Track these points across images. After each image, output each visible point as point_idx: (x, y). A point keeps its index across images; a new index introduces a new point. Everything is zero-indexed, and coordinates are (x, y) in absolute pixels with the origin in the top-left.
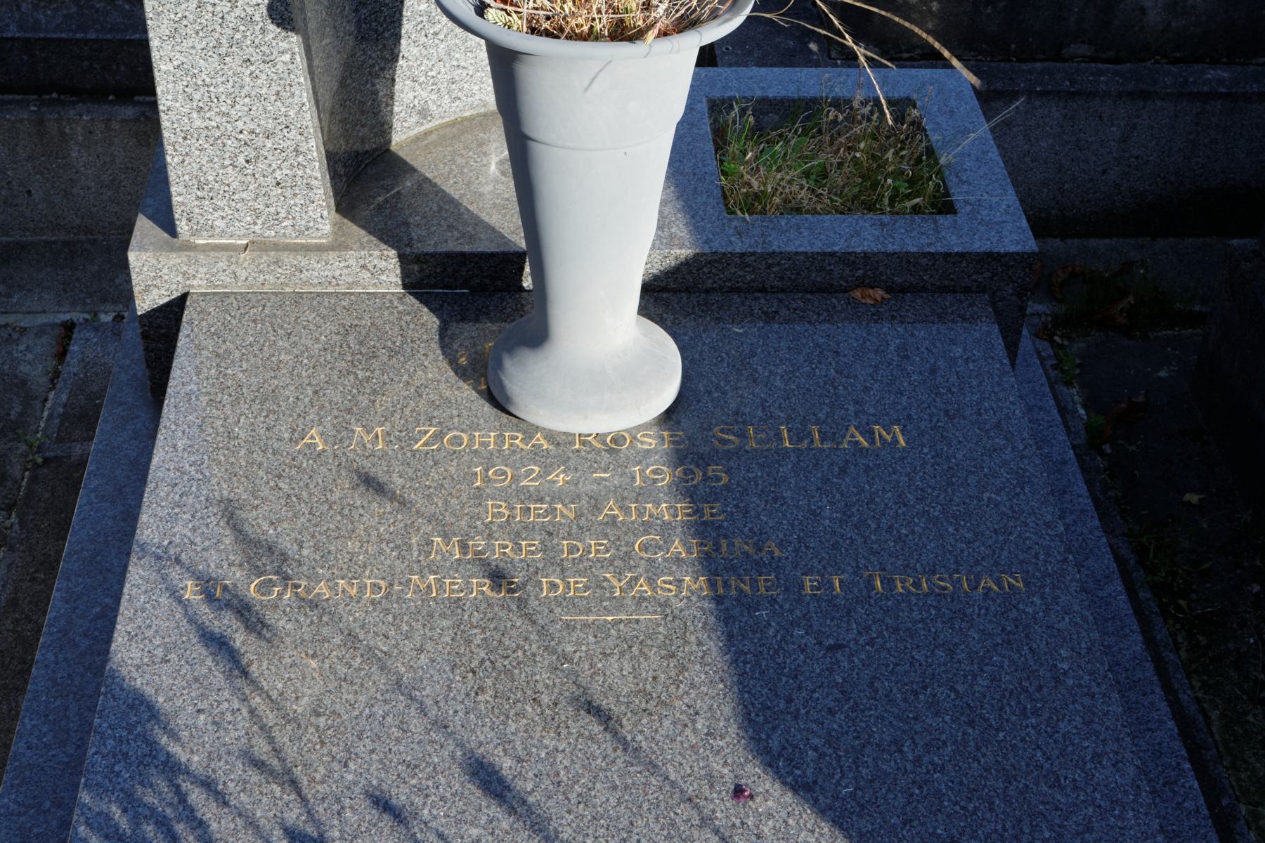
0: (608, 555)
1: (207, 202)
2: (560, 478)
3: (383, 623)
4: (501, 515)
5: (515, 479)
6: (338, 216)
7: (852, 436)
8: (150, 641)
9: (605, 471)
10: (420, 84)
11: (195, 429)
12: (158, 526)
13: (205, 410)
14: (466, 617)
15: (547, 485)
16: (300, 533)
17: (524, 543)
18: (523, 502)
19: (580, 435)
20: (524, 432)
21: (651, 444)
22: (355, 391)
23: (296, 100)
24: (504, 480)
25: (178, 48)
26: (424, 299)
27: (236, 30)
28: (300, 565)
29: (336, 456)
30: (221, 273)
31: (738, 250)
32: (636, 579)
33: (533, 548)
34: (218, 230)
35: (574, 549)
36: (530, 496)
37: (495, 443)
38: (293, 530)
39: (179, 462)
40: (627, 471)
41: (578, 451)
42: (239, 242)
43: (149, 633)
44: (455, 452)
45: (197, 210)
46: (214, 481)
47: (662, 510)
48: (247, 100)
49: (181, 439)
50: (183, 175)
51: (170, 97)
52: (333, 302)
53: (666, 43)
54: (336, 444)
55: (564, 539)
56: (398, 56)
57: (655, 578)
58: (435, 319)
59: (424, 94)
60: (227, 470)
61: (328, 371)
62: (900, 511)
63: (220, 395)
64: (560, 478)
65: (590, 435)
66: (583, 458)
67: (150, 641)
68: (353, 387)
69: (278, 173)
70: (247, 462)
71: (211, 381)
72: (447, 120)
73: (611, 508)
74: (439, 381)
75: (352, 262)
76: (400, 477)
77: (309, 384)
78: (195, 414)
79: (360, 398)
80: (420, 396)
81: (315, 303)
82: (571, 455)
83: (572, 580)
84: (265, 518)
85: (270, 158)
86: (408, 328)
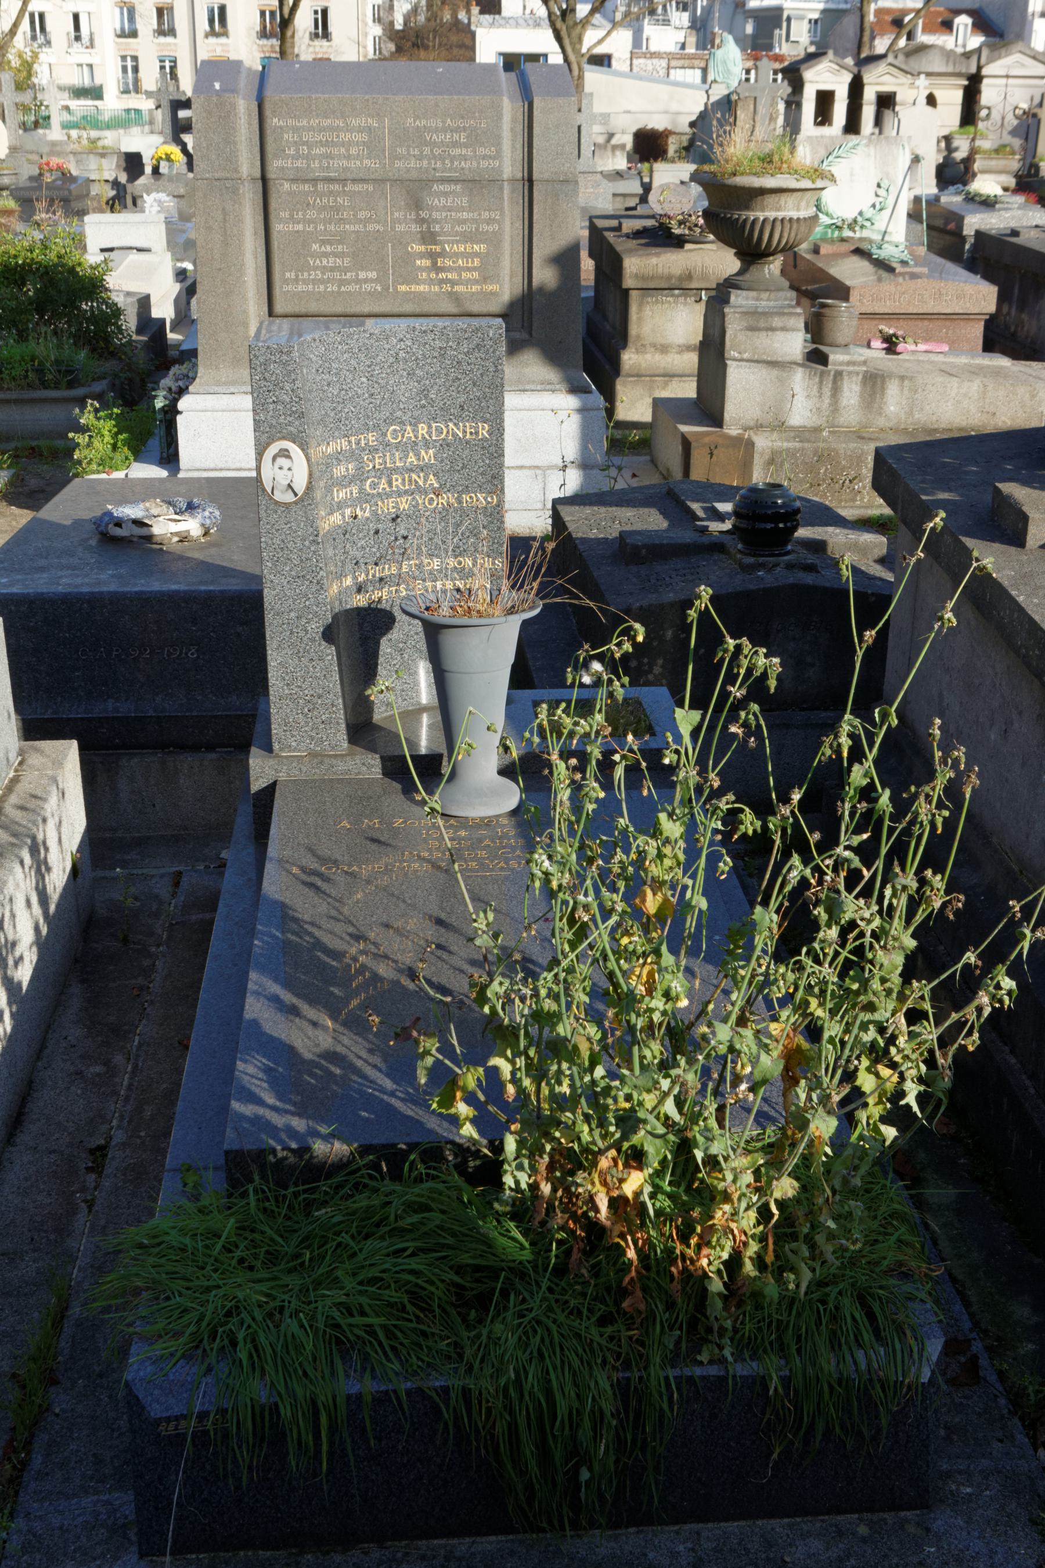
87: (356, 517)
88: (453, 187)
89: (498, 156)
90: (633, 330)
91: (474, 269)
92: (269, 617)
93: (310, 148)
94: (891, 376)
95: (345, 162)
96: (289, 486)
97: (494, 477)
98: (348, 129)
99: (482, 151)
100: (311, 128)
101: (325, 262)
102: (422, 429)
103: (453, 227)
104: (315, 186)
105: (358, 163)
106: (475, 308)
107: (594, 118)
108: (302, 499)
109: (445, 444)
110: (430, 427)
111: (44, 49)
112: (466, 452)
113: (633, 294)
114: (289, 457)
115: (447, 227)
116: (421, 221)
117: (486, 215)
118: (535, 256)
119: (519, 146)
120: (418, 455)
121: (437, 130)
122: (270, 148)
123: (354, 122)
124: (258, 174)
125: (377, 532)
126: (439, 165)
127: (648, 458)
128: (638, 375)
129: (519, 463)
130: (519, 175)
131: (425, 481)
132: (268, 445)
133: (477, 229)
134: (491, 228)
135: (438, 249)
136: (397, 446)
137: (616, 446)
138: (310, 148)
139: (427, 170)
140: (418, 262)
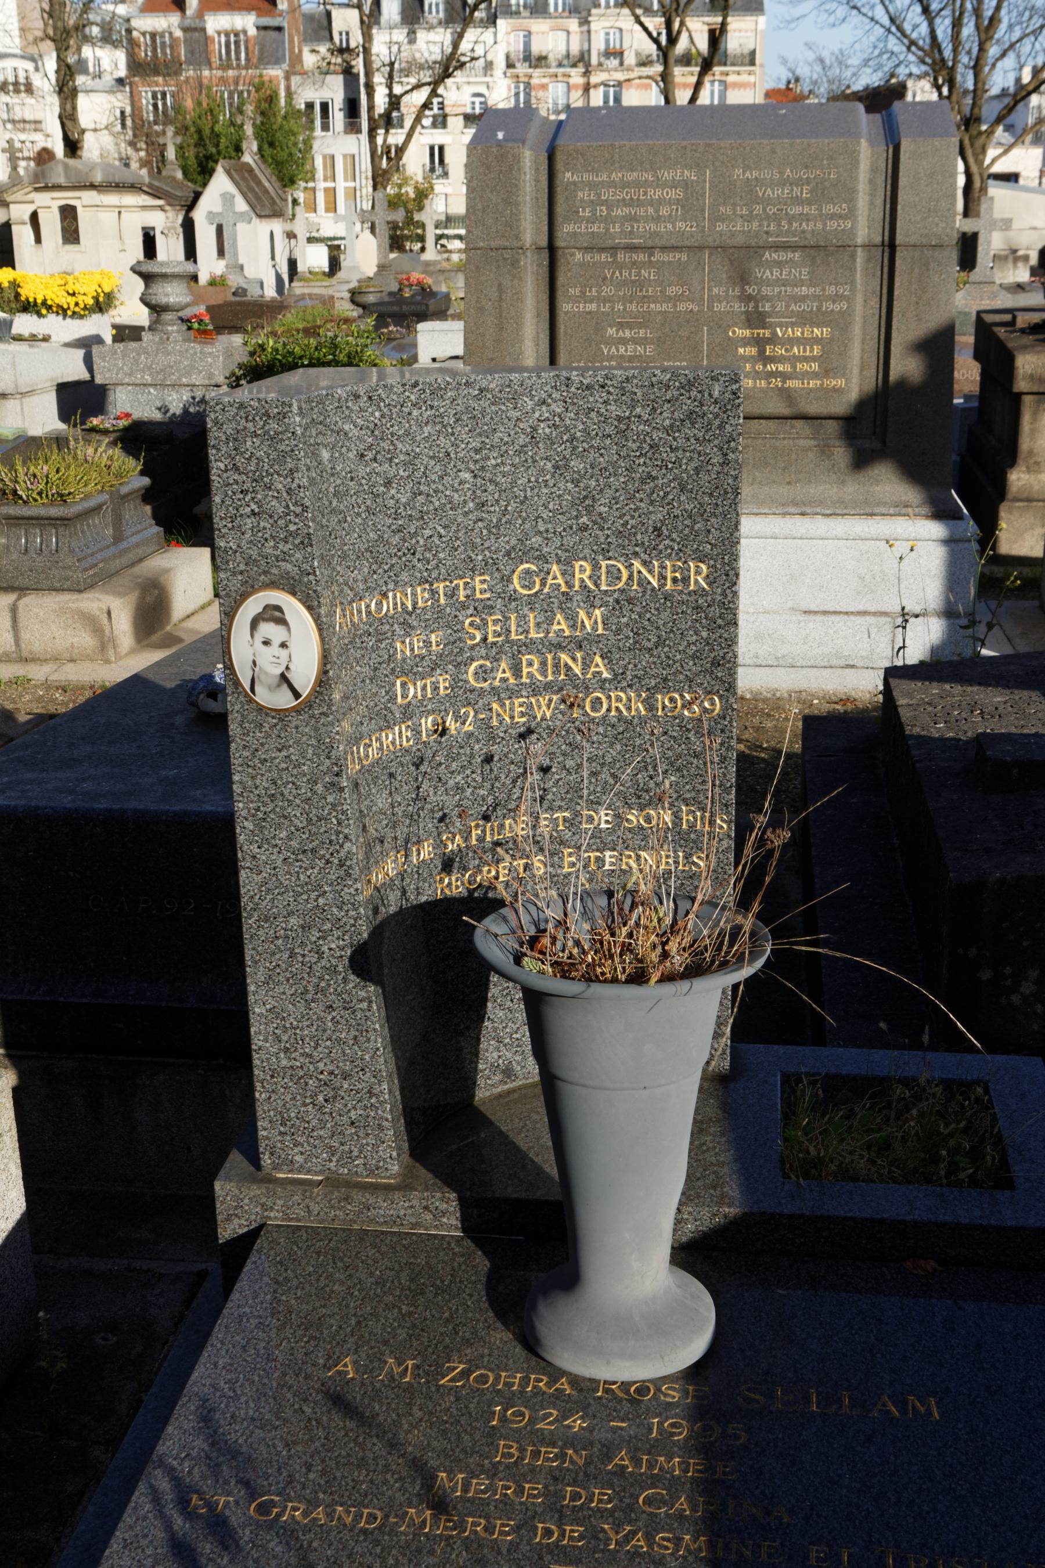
0: (609, 1506)
1: (288, 1138)
2: (577, 1423)
3: (371, 1554)
4: (511, 1455)
5: (532, 1421)
6: (410, 1160)
7: (884, 1405)
8: (143, 1550)
9: (623, 1421)
10: (505, 1045)
11: (238, 1349)
12: (180, 1439)
13: (252, 1332)
14: (454, 1556)
15: (562, 1429)
16: (312, 1457)
17: (527, 1486)
18: (534, 1445)
19: (605, 1382)
20: (550, 1376)
21: (674, 1397)
22: (396, 1324)
23: (372, 1044)
24: (521, 1421)
25: (271, 993)
26: (479, 1243)
27: (321, 979)
28: (304, 1488)
29: (363, 1384)
30: (296, 1206)
31: (786, 1211)
32: (634, 1533)
33: (536, 1492)
34: (297, 1165)
35: (575, 1496)
36: (544, 1439)
37: (520, 1384)
38: (305, 1453)
39: (216, 1378)
40: (646, 1422)
41: (600, 1398)
42: (316, 1178)
43: (144, 1542)
44: (478, 1390)
45: (279, 1145)
46: (243, 1399)
47: (674, 1464)
48: (328, 1043)
49: (224, 1357)
50: (269, 1111)
51: (261, 1038)
52: (394, 1240)
53: (669, 988)
54: (366, 1373)
55: (569, 1485)
56: (484, 1017)
57: (654, 1533)
58: (486, 1262)
59: (509, 1055)
60: (258, 1390)
61: (375, 1303)
62: (924, 1486)
63: (269, 1319)
64: (577, 1423)
65: (615, 1383)
66: (603, 1405)
67: (143, 1550)
68: (394, 1320)
69: (353, 1113)
70: (279, 1384)
71: (264, 1305)
72: (531, 1080)
73: (622, 1458)
74: (478, 1321)
75: (415, 1202)
76: (420, 1410)
77: (355, 1315)
78: (242, 1335)
79: (399, 1331)
80: (457, 1333)
81: (378, 1240)
82: (592, 1402)
83: (568, 1528)
84: (282, 1439)
85: (347, 1098)
86: (460, 1269)
87: (444, 732)
88: (790, 255)
89: (851, 215)
90: (1025, 444)
91: (814, 359)
92: (249, 923)
93: (610, 209)
94: (132, 651)
95: (653, 226)
96: (284, 678)
97: (716, 664)
98: (659, 184)
99: (830, 208)
100: (612, 184)
101: (622, 350)
102: (582, 571)
103: (788, 306)
104: (614, 255)
105: (670, 226)
106: (813, 409)
107: (993, 225)
108: (309, 704)
109: (624, 600)
110: (596, 567)
111: (441, 181)
112: (665, 615)
113: (1027, 400)
114: (282, 621)
115: (780, 306)
116: (746, 299)
117: (831, 290)
118: (893, 342)
119: (879, 201)
120: (572, 620)
121: (772, 184)
122: (560, 209)
123: (667, 175)
124: (544, 242)
125: (488, 759)
126: (773, 227)
127: (1036, 603)
128: (1029, 500)
129: (861, 608)
130: (878, 239)
131: (586, 666)
132: (244, 596)
133: (819, 309)
134: (837, 307)
135: (767, 333)
136: (531, 602)
137: (988, 586)
138: (610, 209)
139: (757, 234)
140: (741, 351)
